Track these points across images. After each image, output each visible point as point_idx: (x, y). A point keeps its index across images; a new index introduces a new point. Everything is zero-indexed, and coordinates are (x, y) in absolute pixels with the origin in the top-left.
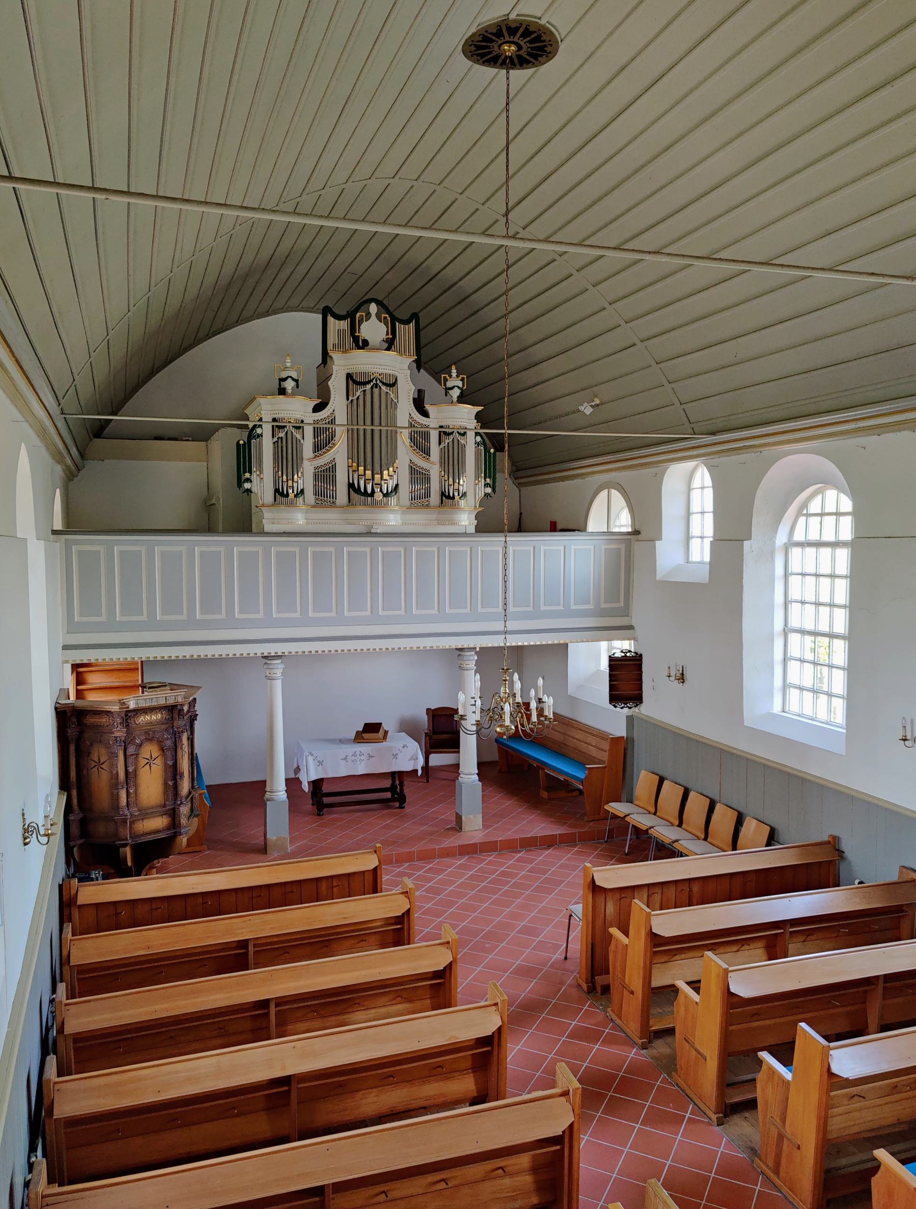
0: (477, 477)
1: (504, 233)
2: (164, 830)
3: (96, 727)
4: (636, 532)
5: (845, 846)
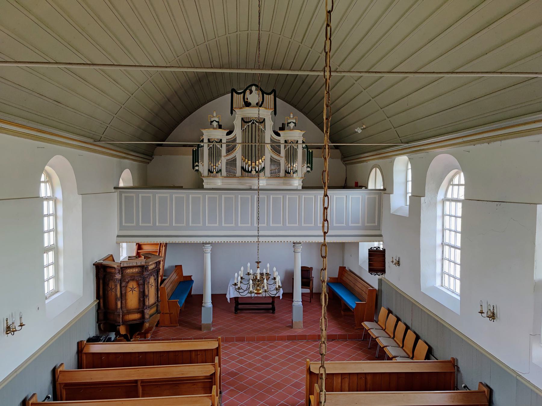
0: (303, 162)
1: (210, 66)
2: (138, 319)
3: (111, 273)
4: (384, 189)
5: (461, 364)
